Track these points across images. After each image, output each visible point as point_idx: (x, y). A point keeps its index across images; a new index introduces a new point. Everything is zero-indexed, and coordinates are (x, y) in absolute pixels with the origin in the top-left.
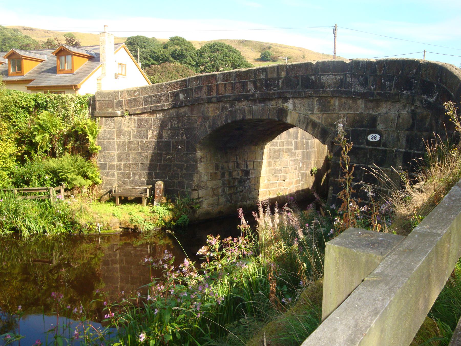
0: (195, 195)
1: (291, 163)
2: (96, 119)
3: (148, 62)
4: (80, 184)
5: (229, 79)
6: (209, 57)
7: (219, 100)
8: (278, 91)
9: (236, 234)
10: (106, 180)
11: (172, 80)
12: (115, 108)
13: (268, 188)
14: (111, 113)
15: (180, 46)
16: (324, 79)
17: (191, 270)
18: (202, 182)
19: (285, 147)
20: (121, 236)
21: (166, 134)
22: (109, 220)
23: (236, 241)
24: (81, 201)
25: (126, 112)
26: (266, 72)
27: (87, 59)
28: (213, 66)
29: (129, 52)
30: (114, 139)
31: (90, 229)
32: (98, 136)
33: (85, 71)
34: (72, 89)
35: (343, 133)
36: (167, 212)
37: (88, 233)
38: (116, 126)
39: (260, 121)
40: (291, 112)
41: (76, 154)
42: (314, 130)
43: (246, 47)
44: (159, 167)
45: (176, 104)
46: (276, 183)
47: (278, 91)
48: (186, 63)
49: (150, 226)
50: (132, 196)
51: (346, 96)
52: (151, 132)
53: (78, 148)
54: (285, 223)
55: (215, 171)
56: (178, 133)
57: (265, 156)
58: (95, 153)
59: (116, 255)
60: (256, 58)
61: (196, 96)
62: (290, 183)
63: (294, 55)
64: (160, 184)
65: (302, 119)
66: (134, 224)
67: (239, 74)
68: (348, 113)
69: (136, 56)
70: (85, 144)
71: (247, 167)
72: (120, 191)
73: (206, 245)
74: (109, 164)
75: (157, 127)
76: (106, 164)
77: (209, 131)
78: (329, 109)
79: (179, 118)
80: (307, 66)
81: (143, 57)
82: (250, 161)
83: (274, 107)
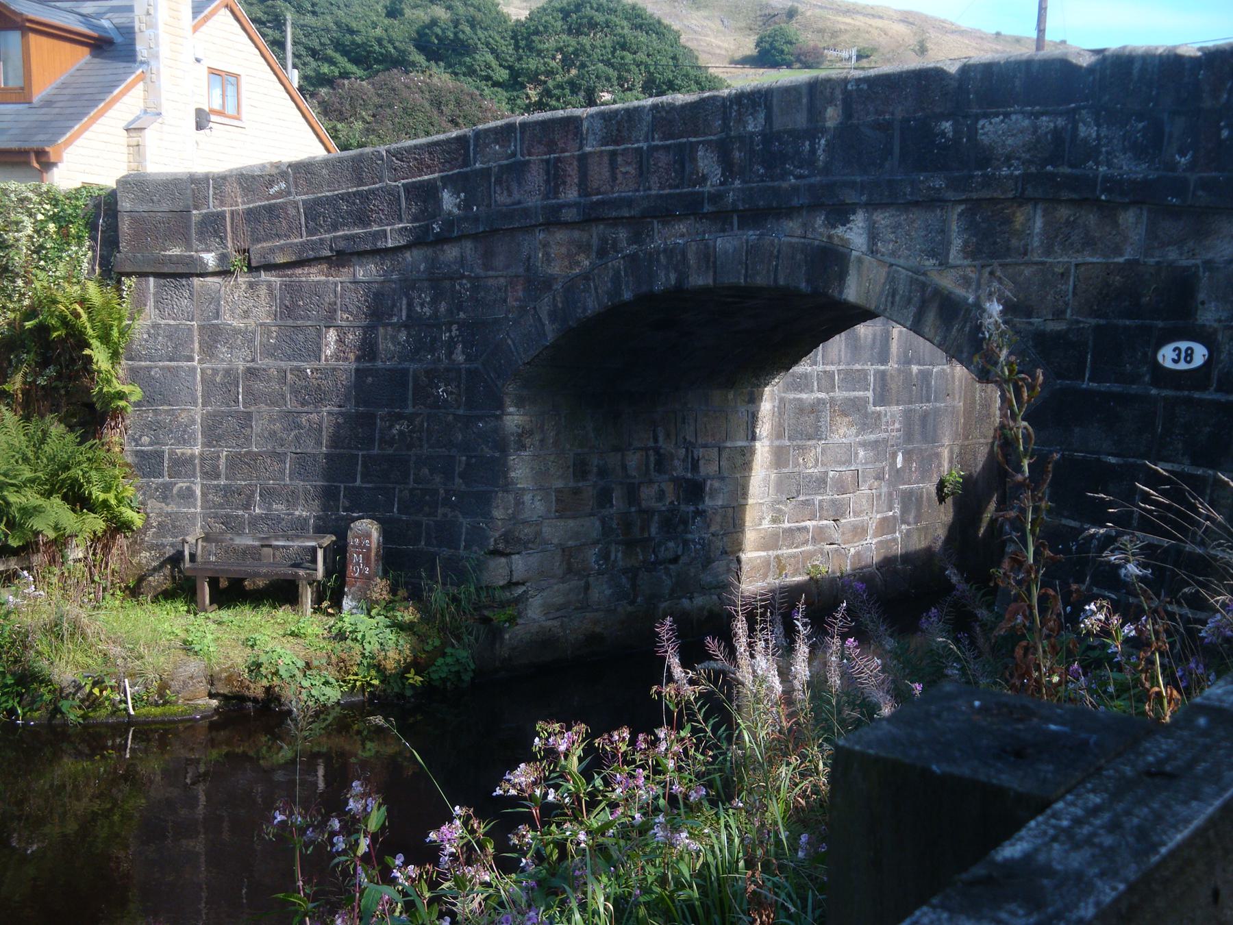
0: (497, 572)
1: (861, 453)
2: (119, 282)
3: (325, 69)
4: (56, 528)
5: (625, 134)
6: (560, 50)
7: (590, 216)
8: (813, 180)
9: (646, 718)
10: (159, 515)
11: (416, 136)
12: (195, 243)
13: (776, 547)
14: (179, 260)
15: (449, 8)
16: (990, 130)
17: (469, 855)
18: (525, 522)
19: (839, 394)
20: (213, 726)
21: (390, 343)
22: (168, 667)
23: (644, 746)
24: (57, 594)
25: (237, 259)
26: (769, 109)
27: (86, 50)
28: (574, 87)
29: (252, 27)
30: (191, 359)
31: (92, 703)
32: (128, 348)
33: (76, 97)
34: (27, 164)
35: (1002, 334)
36: (393, 637)
37: (84, 717)
38: (197, 313)
39: (745, 294)
40: (859, 260)
41: (42, 417)
42: (948, 329)
43: (704, 13)
44: (364, 464)
45: (427, 229)
46: (806, 529)
47: (813, 180)
48: (471, 72)
49: (328, 690)
50: (257, 575)
51: (1075, 196)
52: (332, 335)
53: (48, 391)
54: (835, 680)
55: (571, 484)
56: (434, 339)
57: (764, 428)
58: (118, 413)
59: (192, 802)
60: (739, 55)
61: (502, 198)
62: (859, 531)
63: (883, 40)
64: (367, 532)
65: (902, 289)
66: (265, 682)
67: (664, 118)
68: (1080, 260)
69: (278, 45)
70: (77, 377)
71: (695, 466)
72: (213, 558)
73: (530, 758)
74: (172, 453)
75: (355, 317)
76: (159, 455)
77: (551, 332)
78: (1008, 249)
79: (437, 281)
80: (925, 82)
81: (308, 48)
82: (705, 446)
83: (794, 240)
